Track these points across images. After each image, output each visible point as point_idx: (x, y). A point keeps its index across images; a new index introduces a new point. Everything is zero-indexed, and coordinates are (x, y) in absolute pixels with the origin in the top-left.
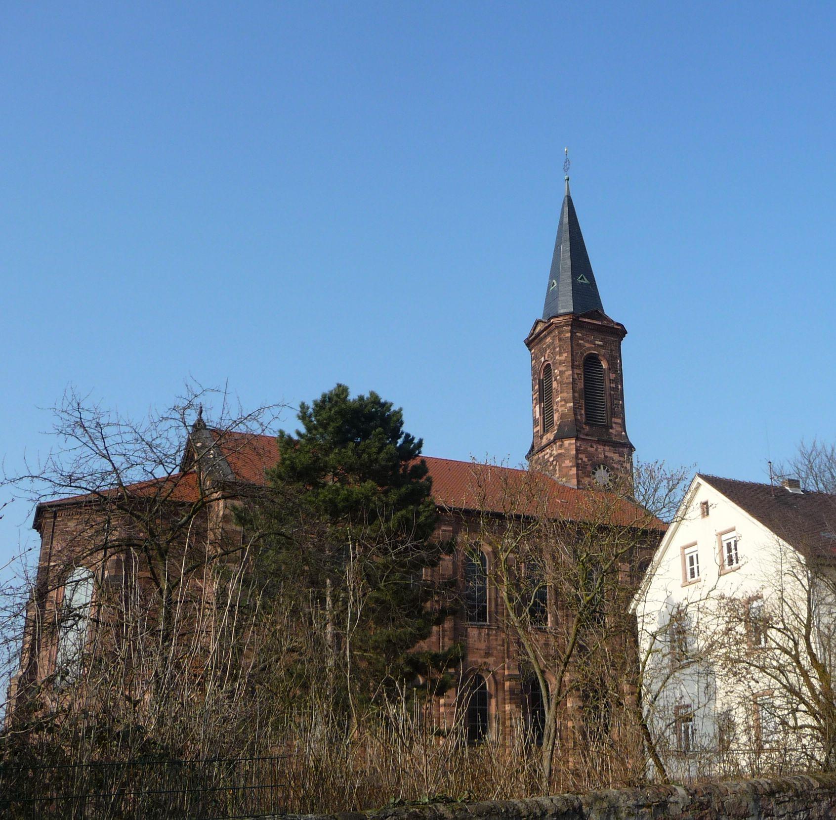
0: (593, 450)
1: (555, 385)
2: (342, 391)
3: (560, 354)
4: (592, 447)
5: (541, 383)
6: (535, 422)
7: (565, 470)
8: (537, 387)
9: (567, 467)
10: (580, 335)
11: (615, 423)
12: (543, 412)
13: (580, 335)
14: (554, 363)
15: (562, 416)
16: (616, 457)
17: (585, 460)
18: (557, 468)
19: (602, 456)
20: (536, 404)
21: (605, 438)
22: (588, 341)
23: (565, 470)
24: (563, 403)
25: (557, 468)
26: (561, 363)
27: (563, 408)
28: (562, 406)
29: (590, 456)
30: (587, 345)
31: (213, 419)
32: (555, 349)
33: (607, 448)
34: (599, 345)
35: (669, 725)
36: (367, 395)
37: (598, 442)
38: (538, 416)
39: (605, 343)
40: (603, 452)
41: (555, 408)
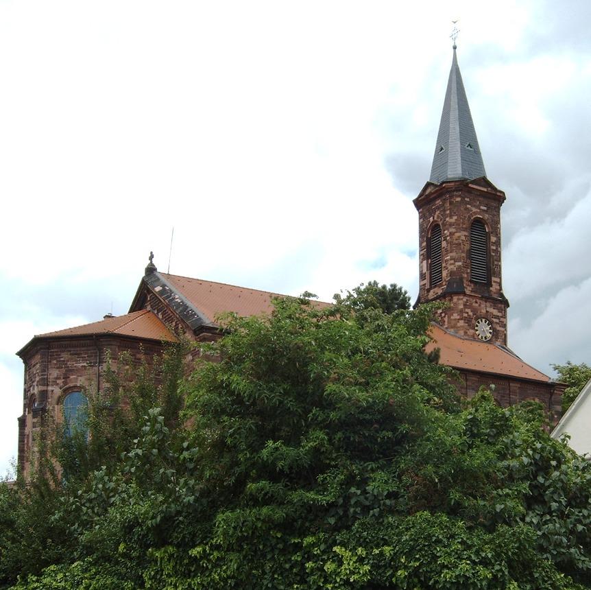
0: (477, 305)
1: (444, 244)
2: (375, 283)
3: (451, 216)
4: (476, 302)
5: (429, 241)
6: (422, 277)
7: (453, 322)
8: (424, 244)
9: (455, 319)
10: (468, 200)
11: (495, 282)
12: (430, 267)
13: (468, 200)
14: (444, 225)
15: (452, 273)
16: (495, 312)
17: (471, 314)
18: (446, 319)
19: (484, 311)
20: (423, 260)
21: (487, 295)
22: (474, 206)
23: (453, 322)
24: (452, 262)
25: (446, 319)
26: (451, 225)
27: (452, 266)
28: (451, 264)
29: (474, 311)
30: (474, 210)
31: (161, 268)
32: (444, 211)
33: (488, 304)
34: (484, 210)
35: (177, 328)
36: (389, 287)
37: (481, 298)
38: (425, 271)
39: (488, 208)
40: (486, 308)
41: (444, 265)
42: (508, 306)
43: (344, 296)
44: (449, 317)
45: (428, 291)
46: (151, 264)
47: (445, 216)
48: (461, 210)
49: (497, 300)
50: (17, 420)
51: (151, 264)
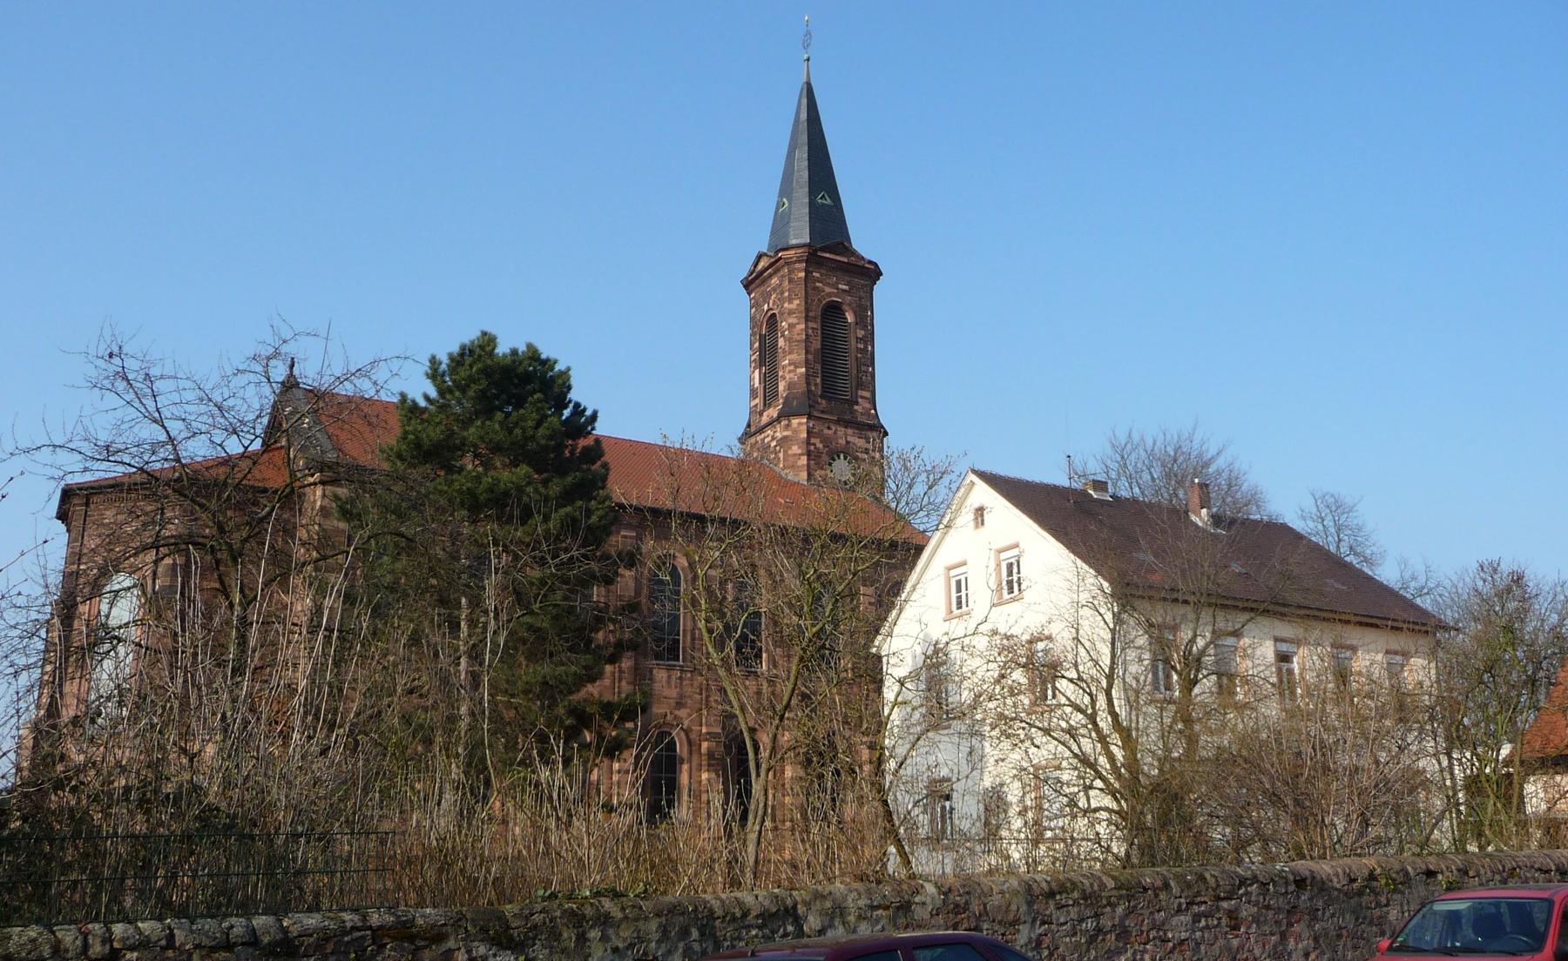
1: (781, 342)
2: (488, 341)
3: (790, 300)
5: (762, 339)
15: (790, 386)
21: (848, 417)
30: (828, 290)
33: (850, 431)
37: (838, 422)
40: (844, 435)
42: (886, 434)
43: (502, 349)
44: (785, 452)
45: (761, 414)
46: (291, 375)
47: (782, 300)
48: (125, 377)
49: (864, 424)
50: (470, 335)
51: (291, 375)
